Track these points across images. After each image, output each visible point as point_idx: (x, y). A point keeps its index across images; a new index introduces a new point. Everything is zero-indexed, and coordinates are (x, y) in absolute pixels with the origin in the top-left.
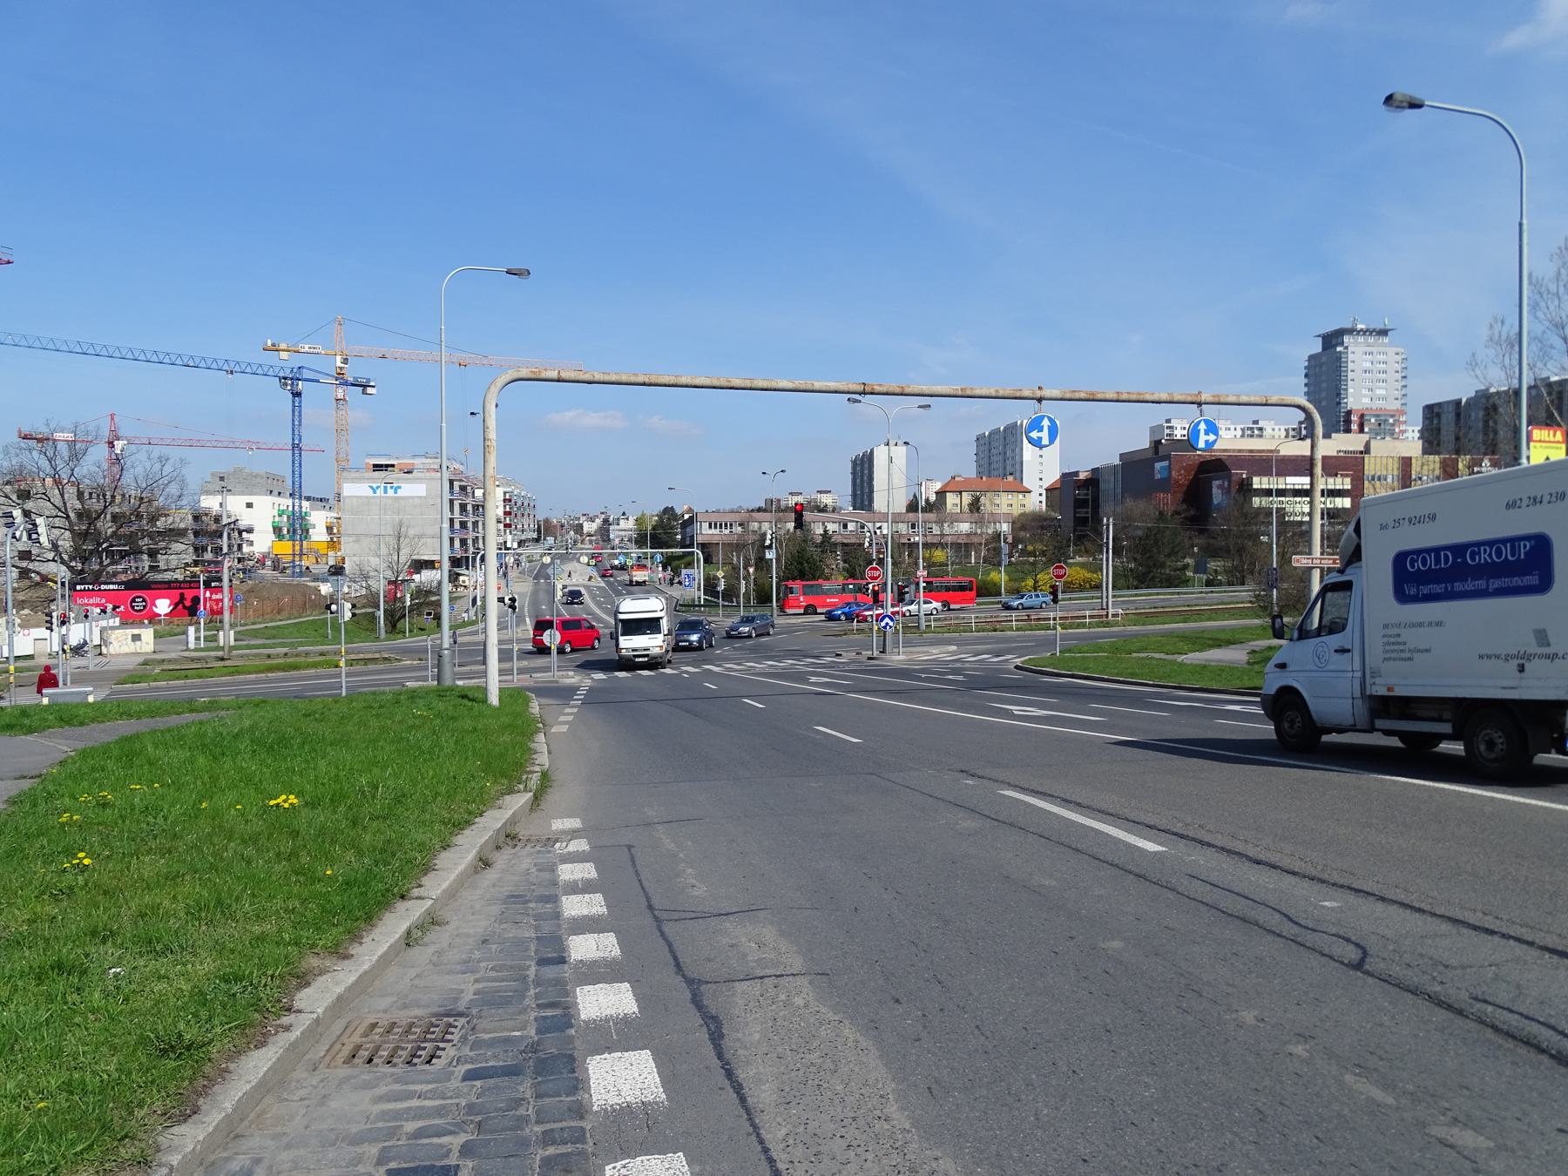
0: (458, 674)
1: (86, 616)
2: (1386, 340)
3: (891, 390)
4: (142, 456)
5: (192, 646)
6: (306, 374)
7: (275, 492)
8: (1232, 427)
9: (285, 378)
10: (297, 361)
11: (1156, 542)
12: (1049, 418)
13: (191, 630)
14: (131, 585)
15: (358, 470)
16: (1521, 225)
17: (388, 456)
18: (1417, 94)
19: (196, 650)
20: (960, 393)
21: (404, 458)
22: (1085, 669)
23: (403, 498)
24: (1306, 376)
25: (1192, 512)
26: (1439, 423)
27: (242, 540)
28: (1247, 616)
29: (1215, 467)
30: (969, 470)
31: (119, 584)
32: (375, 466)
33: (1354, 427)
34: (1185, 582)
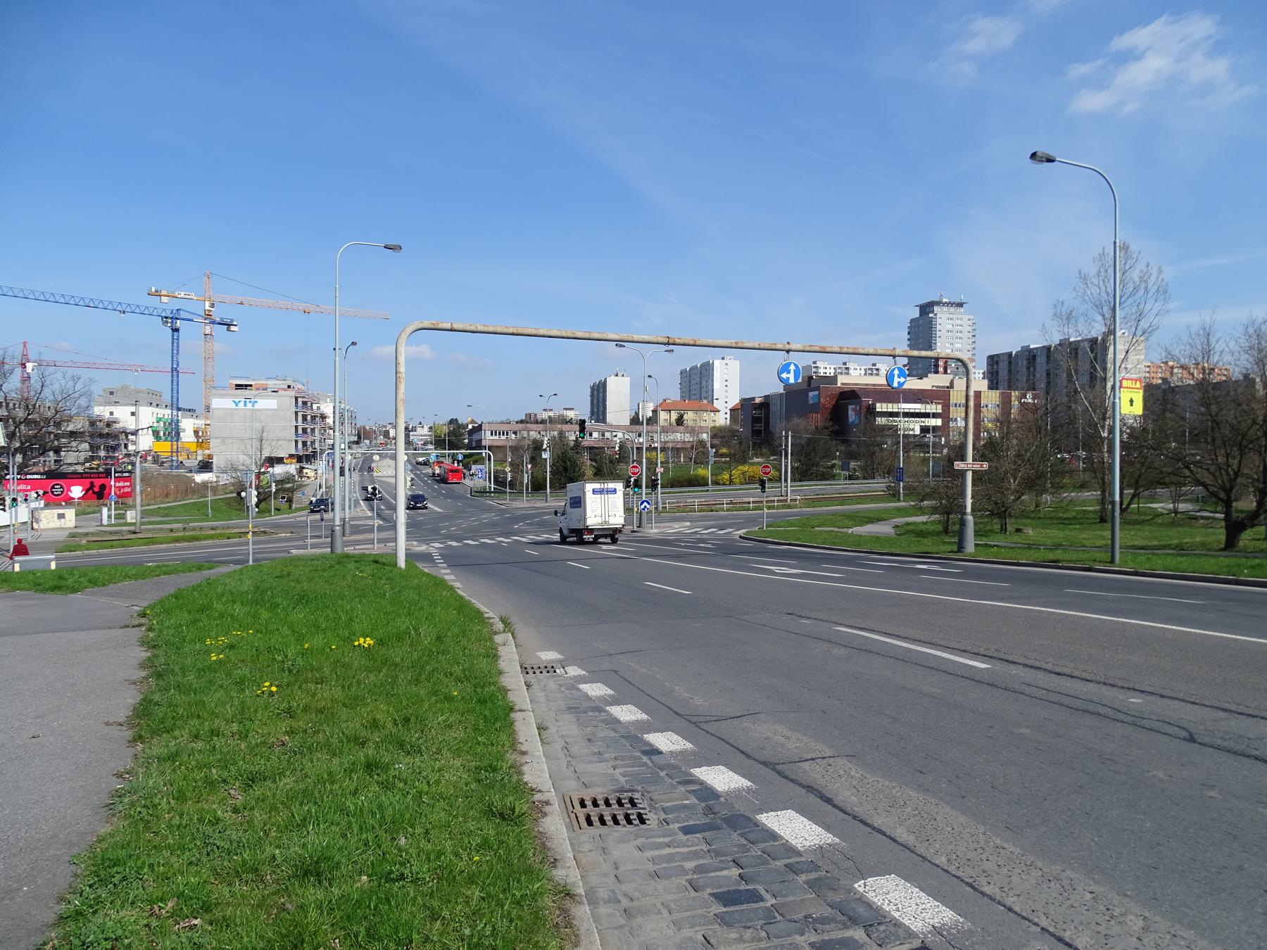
0: (347, 542)
1: (26, 500)
2: (962, 310)
3: (687, 342)
4: (59, 375)
5: (105, 522)
6: (183, 315)
7: (154, 404)
8: (858, 368)
9: (166, 318)
10: (176, 305)
11: (814, 450)
12: (795, 364)
13: (105, 510)
14: (51, 475)
15: (224, 388)
16: (1115, 243)
17: (248, 378)
18: (1051, 152)
19: (108, 526)
20: (734, 345)
21: (260, 379)
22: (797, 540)
23: (259, 410)
24: (909, 333)
25: (836, 427)
26: (998, 368)
27: (128, 440)
28: (882, 501)
29: (850, 395)
30: (675, 394)
31: (41, 474)
32: (237, 385)
33: (941, 369)
34: (833, 477)
